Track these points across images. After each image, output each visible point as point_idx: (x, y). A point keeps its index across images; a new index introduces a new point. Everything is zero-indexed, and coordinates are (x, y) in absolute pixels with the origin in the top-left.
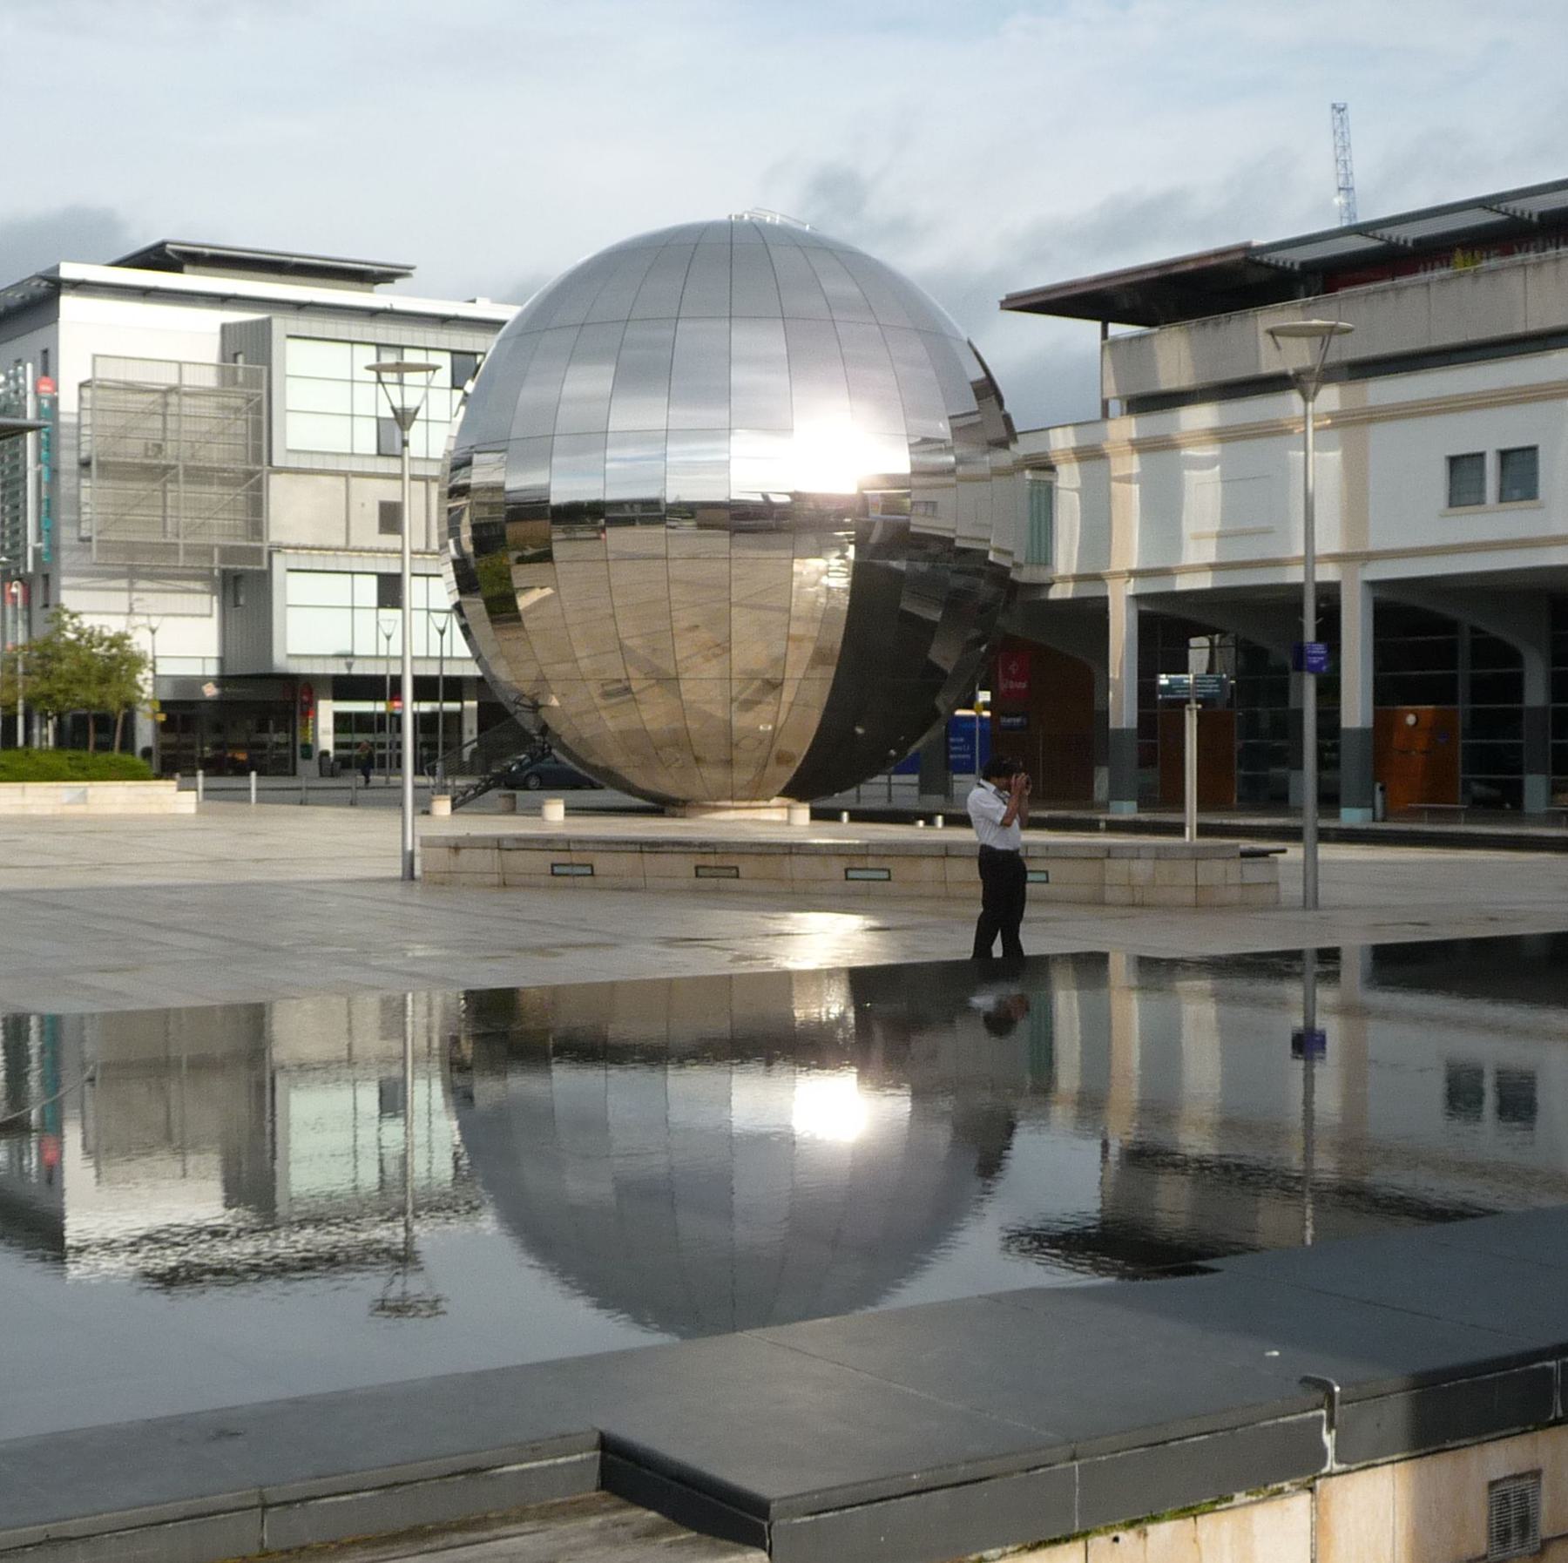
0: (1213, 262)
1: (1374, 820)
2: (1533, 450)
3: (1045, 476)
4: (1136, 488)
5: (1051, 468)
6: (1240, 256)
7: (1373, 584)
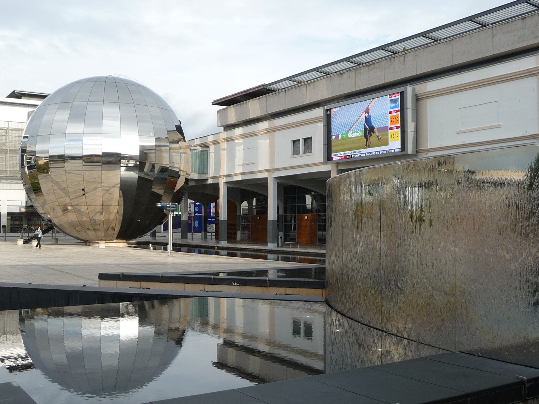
0: (257, 89)
1: (278, 247)
2: (311, 138)
3: (206, 149)
4: (226, 152)
5: (208, 147)
6: (262, 87)
7: (277, 178)
